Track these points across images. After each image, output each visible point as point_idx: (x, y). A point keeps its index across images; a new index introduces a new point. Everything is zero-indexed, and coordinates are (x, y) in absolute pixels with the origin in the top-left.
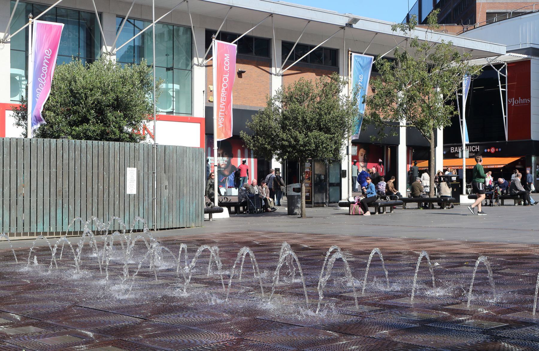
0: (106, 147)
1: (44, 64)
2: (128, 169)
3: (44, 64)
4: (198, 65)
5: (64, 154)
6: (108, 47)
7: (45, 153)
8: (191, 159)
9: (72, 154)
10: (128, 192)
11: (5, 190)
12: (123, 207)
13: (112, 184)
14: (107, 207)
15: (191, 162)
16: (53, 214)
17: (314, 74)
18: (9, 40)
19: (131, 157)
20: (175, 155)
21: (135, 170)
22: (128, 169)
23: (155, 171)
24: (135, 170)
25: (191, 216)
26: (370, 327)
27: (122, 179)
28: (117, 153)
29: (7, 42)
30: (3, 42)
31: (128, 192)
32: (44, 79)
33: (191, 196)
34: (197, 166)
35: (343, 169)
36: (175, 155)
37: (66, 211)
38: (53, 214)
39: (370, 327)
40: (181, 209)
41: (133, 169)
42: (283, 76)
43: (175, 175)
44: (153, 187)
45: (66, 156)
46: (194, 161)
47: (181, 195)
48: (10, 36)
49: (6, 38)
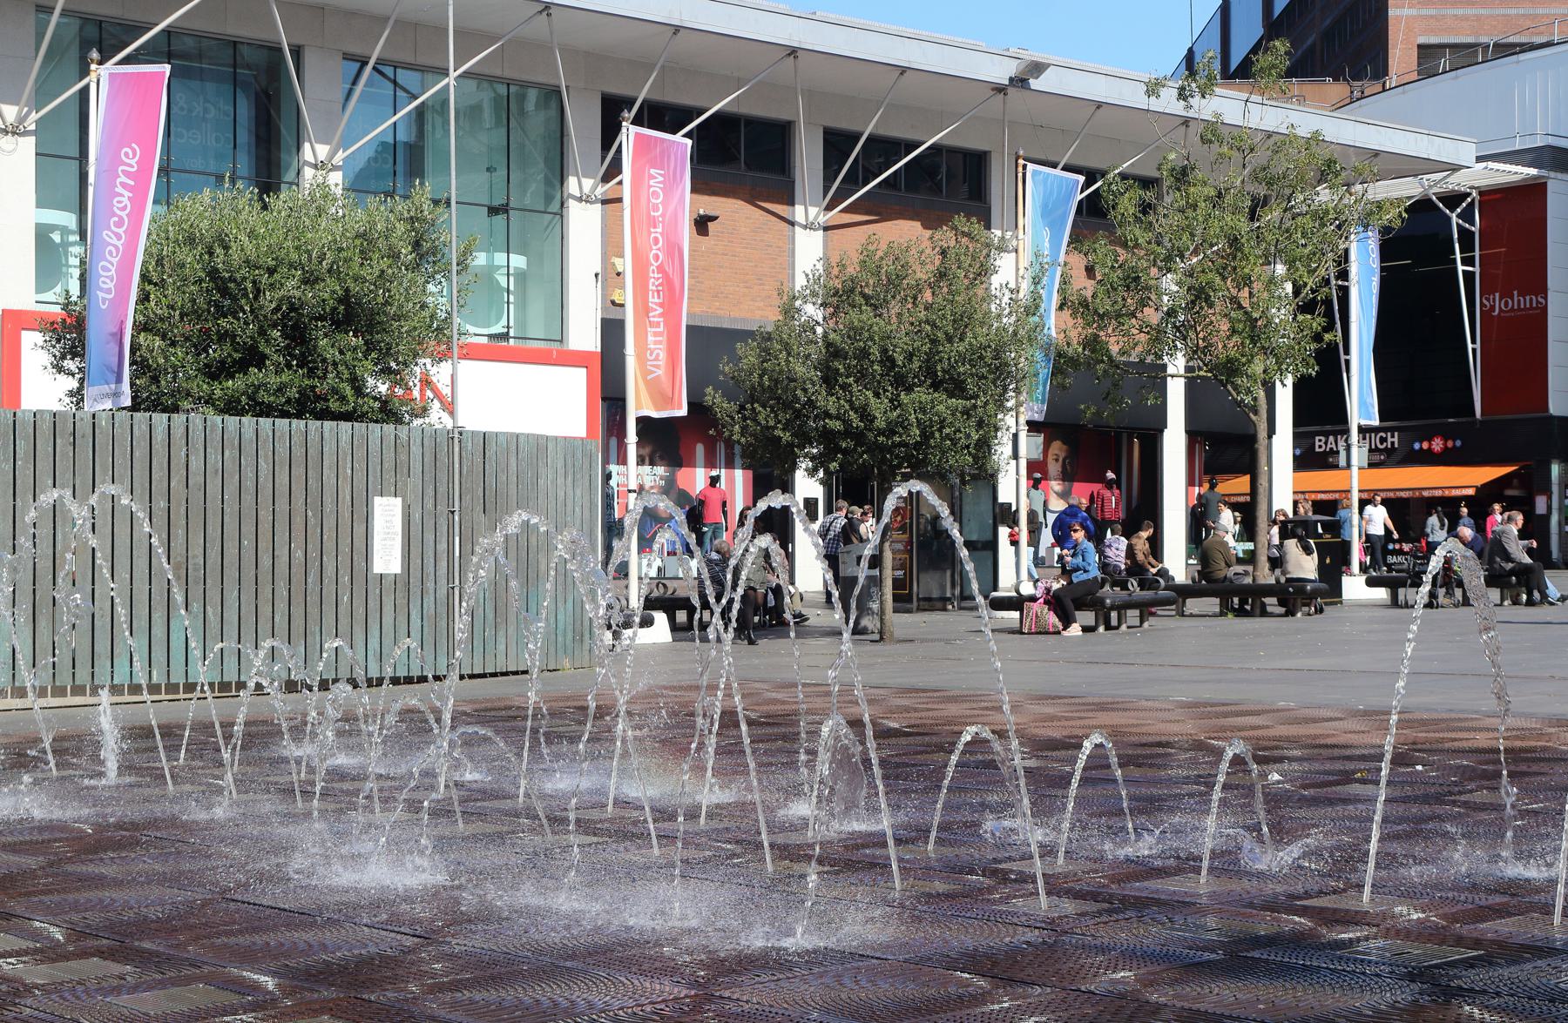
0: (313, 436)
1: (119, 189)
2: (378, 500)
3: (119, 189)
4: (580, 199)
6: (318, 147)
7: (137, 454)
8: (561, 471)
9: (214, 458)
10: (378, 567)
12: (362, 610)
13: (329, 545)
15: (560, 480)
17: (918, 224)
18: (33, 127)
19: (386, 465)
20: (513, 461)
22: (378, 500)
23: (457, 508)
25: (560, 639)
27: (359, 530)
28: (345, 454)
29: (26, 133)
30: (14, 133)
31: (378, 567)
34: (578, 492)
36: (513, 461)
41: (392, 500)
42: (826, 229)
44: (450, 551)
45: (196, 463)
46: (570, 478)
48: (34, 116)
49: (22, 119)
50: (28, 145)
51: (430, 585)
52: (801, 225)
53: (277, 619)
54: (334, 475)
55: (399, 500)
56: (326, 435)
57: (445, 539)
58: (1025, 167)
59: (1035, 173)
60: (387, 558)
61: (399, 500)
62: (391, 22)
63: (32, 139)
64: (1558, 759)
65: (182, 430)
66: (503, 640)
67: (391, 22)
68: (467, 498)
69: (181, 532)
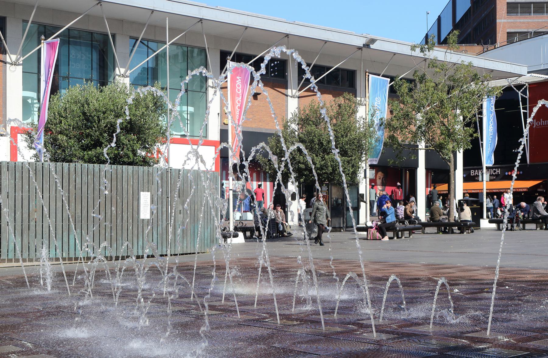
0: (119, 171)
2: (142, 193)
5: (77, 178)
6: (12, 56)
9: (85, 179)
10: (142, 216)
12: (136, 232)
13: (125, 209)
14: (121, 232)
18: (21, 63)
19: (145, 181)
22: (142, 193)
25: (206, 242)
29: (19, 65)
30: (15, 65)
31: (142, 216)
33: (206, 221)
42: (299, 97)
45: (78, 180)
48: (22, 59)
49: (18, 60)
51: (160, 223)
52: (9, 63)
55: (149, 193)
56: (124, 170)
57: (165, 207)
61: (149, 193)
62: (146, 25)
65: (73, 169)
67: (146, 25)
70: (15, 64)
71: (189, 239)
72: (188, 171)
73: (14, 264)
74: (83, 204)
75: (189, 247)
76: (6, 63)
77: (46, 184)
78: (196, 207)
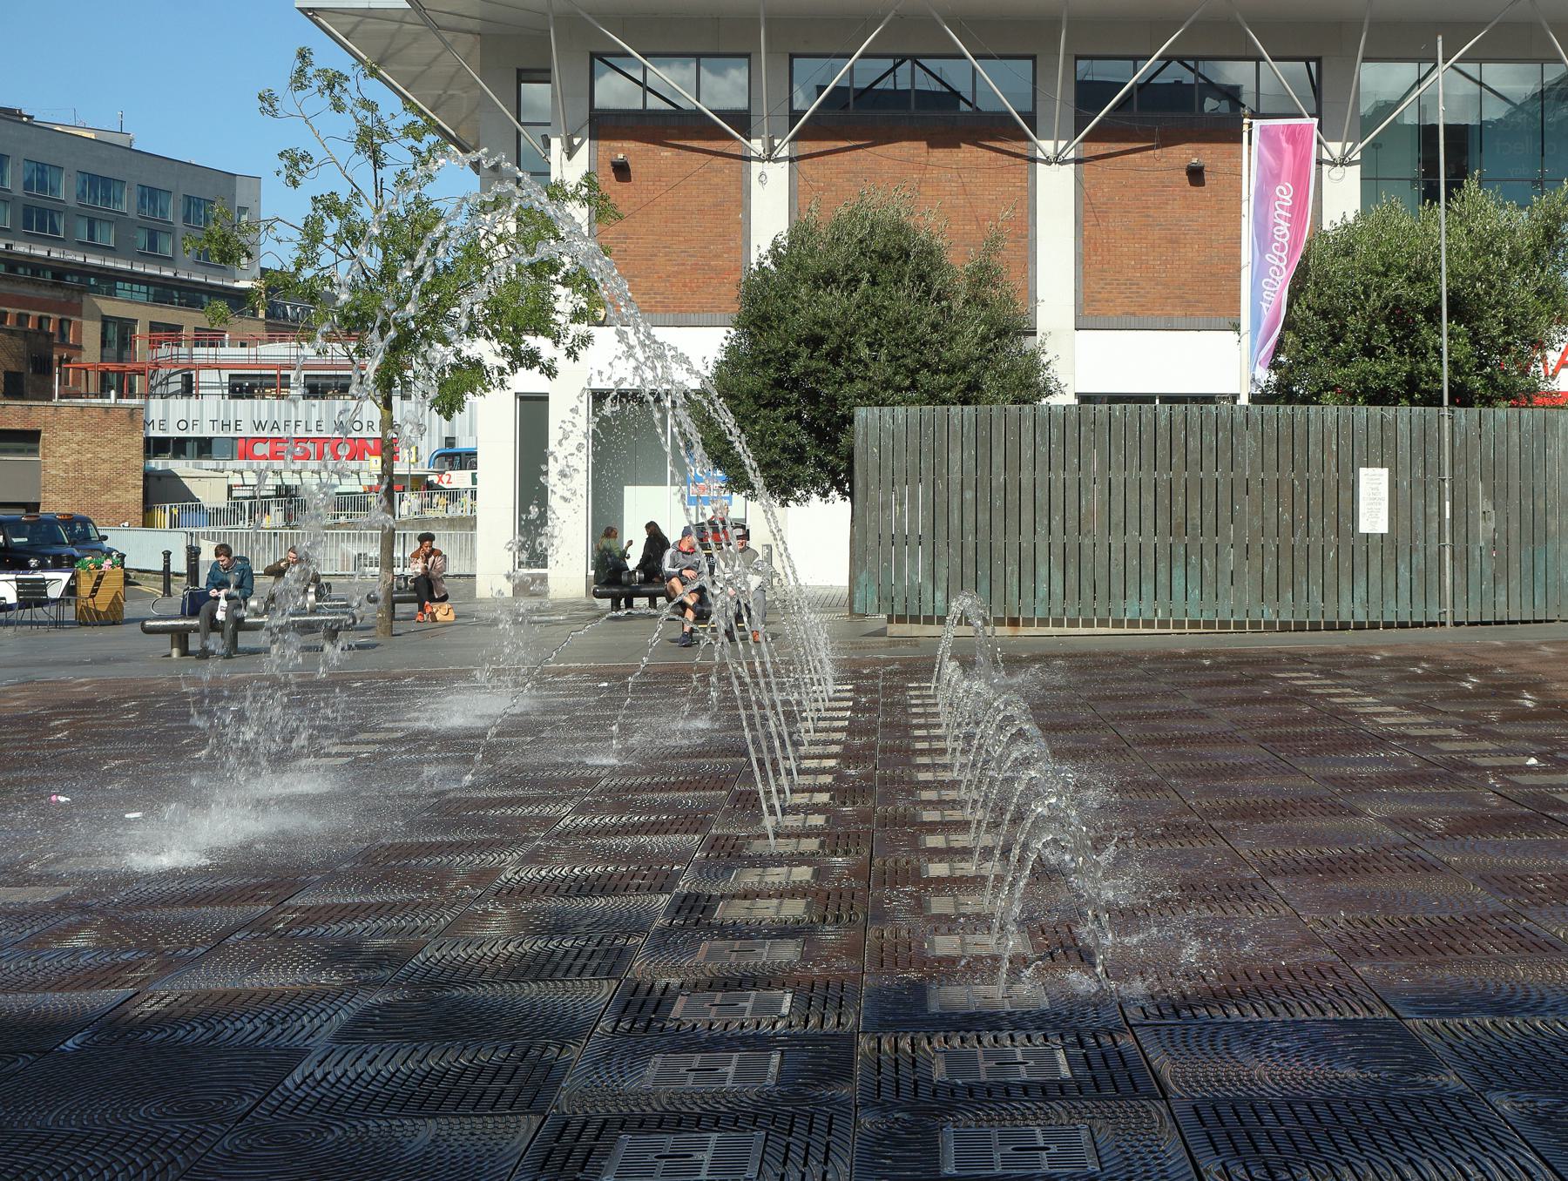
0: (1299, 417)
5: (1190, 439)
6: (1331, 145)
9: (1209, 438)
10: (1365, 527)
11: (1053, 523)
12: (1348, 564)
13: (1315, 509)
14: (1304, 563)
16: (1163, 578)
17: (924, 144)
18: (1358, 157)
19: (1372, 441)
20: (1515, 434)
21: (1383, 473)
24: (1383, 473)
26: (239, 1025)
27: (1345, 496)
28: (1331, 433)
29: (1351, 163)
30: (1342, 164)
31: (1365, 527)
32: (1283, 255)
35: (1385, 471)
36: (1515, 434)
37: (1194, 573)
38: (1163, 578)
39: (239, 1025)
40: (1540, 574)
41: (1378, 470)
42: (1077, 161)
43: (1515, 483)
44: (1441, 514)
45: (1193, 443)
47: (1539, 534)
50: (1355, 171)
51: (1420, 543)
52: (1328, 162)
53: (1266, 570)
54: (1319, 451)
56: (1312, 417)
58: (1250, 125)
59: (1263, 130)
60: (1374, 516)
61: (1385, 471)
62: (1366, 26)
63: (1358, 168)
64: (1560, 806)
65: (1181, 417)
66: (1504, 593)
67: (1366, 26)
68: (1460, 469)
69: (1181, 499)
70: (1058, 160)
71: (1514, 583)
72: (759, 462)
73: (1066, 630)
74: (1205, 497)
75: (1515, 601)
76: (1034, 160)
77: (1118, 452)
78: (1541, 504)
